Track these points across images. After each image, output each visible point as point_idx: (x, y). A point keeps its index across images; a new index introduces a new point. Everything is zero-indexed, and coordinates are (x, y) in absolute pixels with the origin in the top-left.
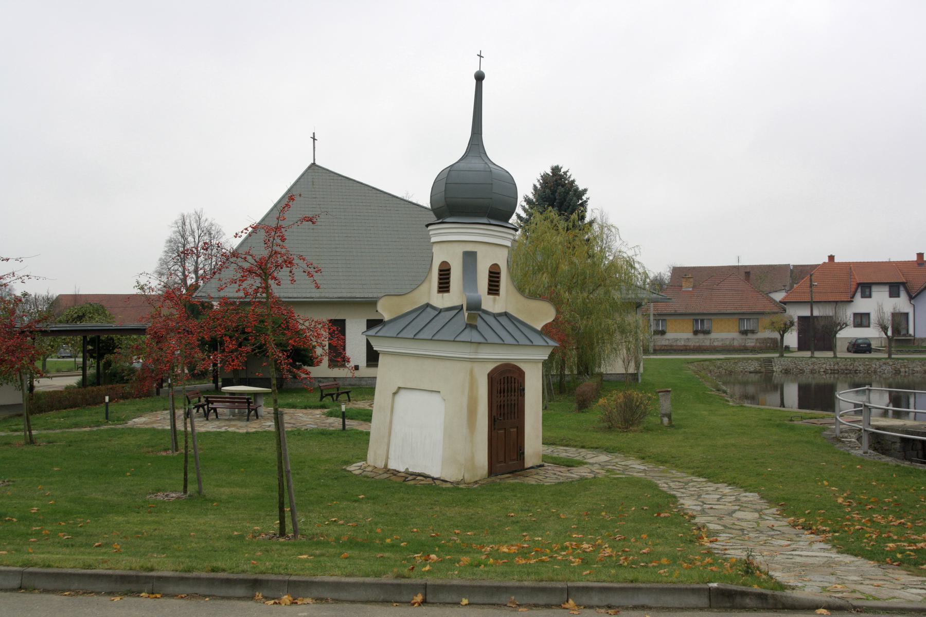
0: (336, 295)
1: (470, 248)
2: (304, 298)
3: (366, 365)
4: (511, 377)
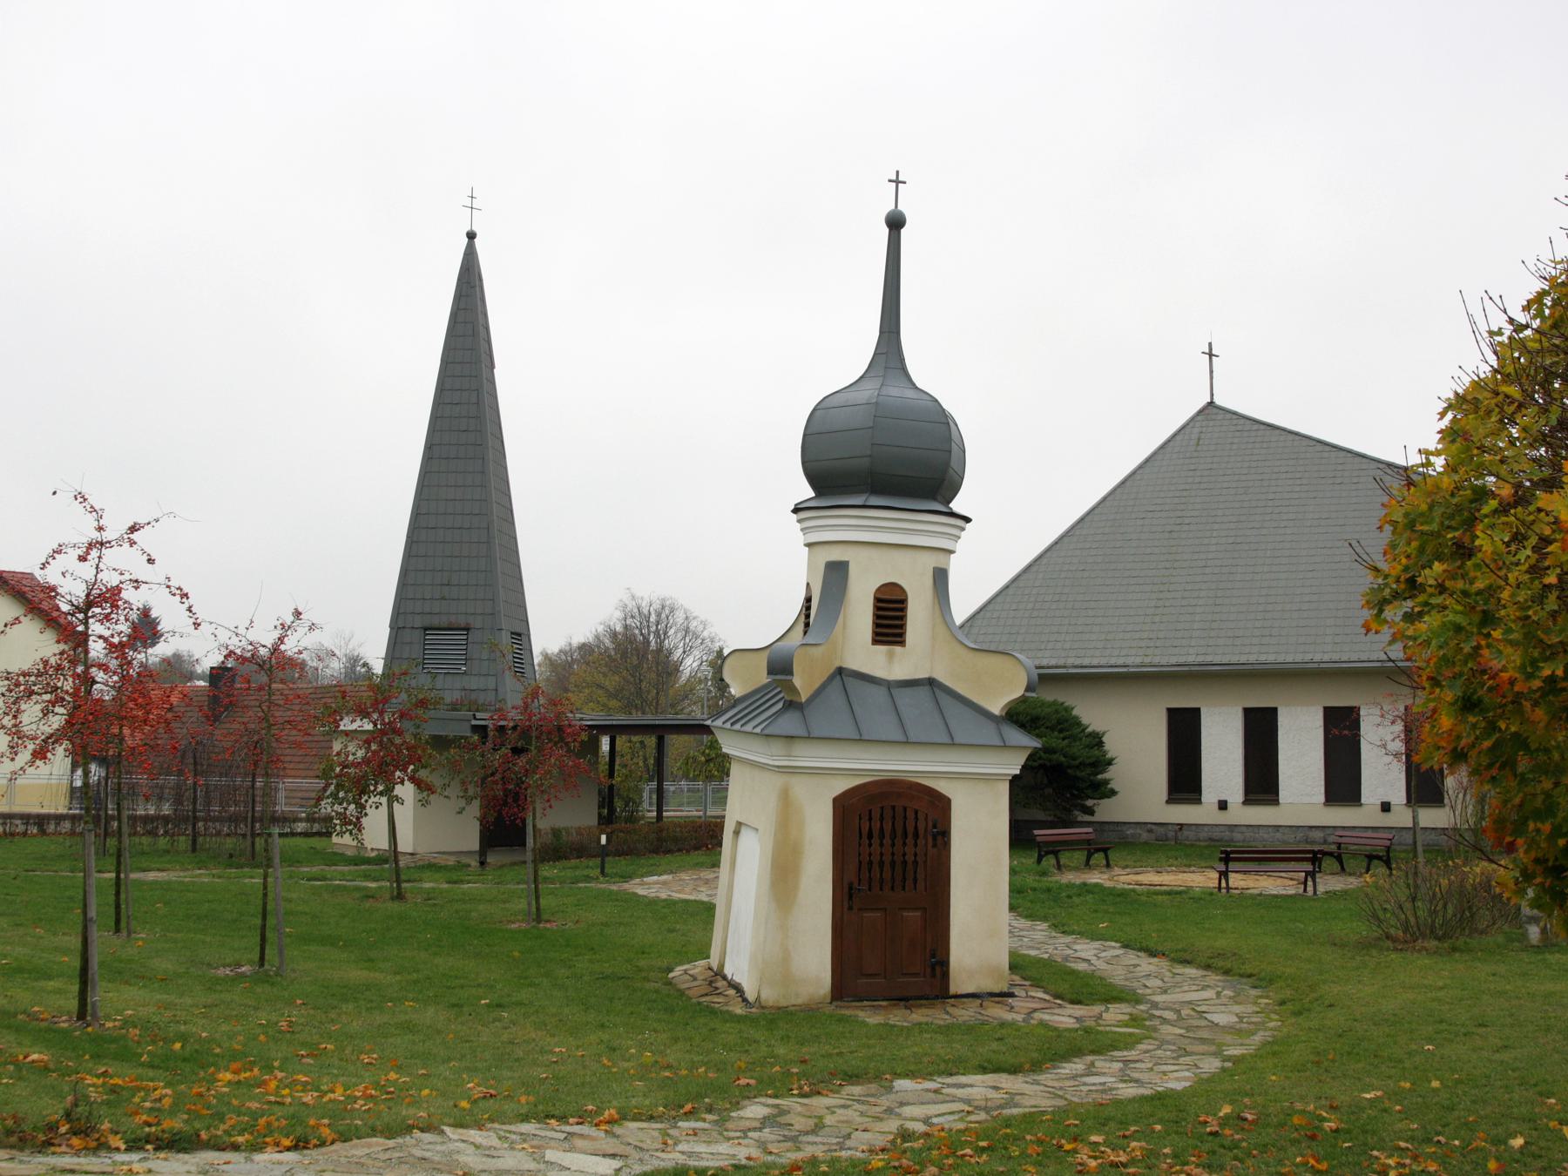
0: (1173, 660)
1: (836, 555)
2: (1112, 666)
3: (1322, 798)
4: (905, 809)
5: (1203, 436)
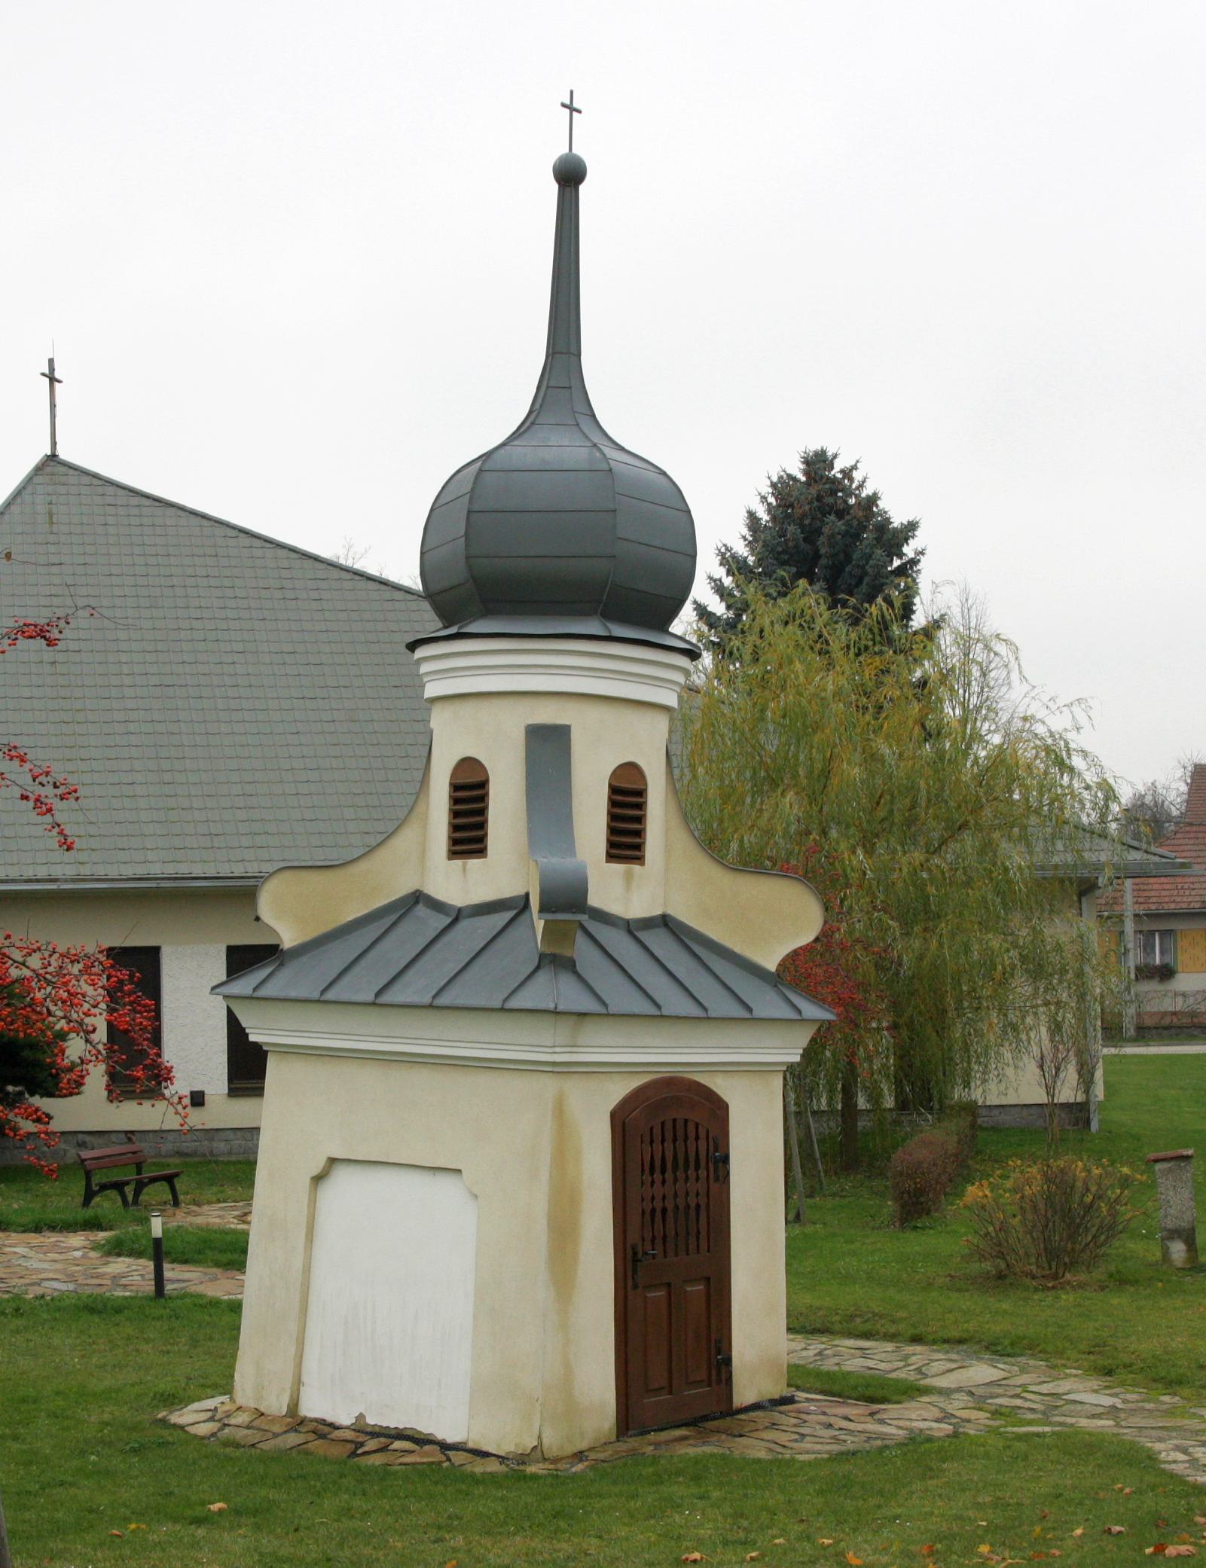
0: (128, 871)
1: (547, 714)
4: (686, 1121)
5: (54, 509)
